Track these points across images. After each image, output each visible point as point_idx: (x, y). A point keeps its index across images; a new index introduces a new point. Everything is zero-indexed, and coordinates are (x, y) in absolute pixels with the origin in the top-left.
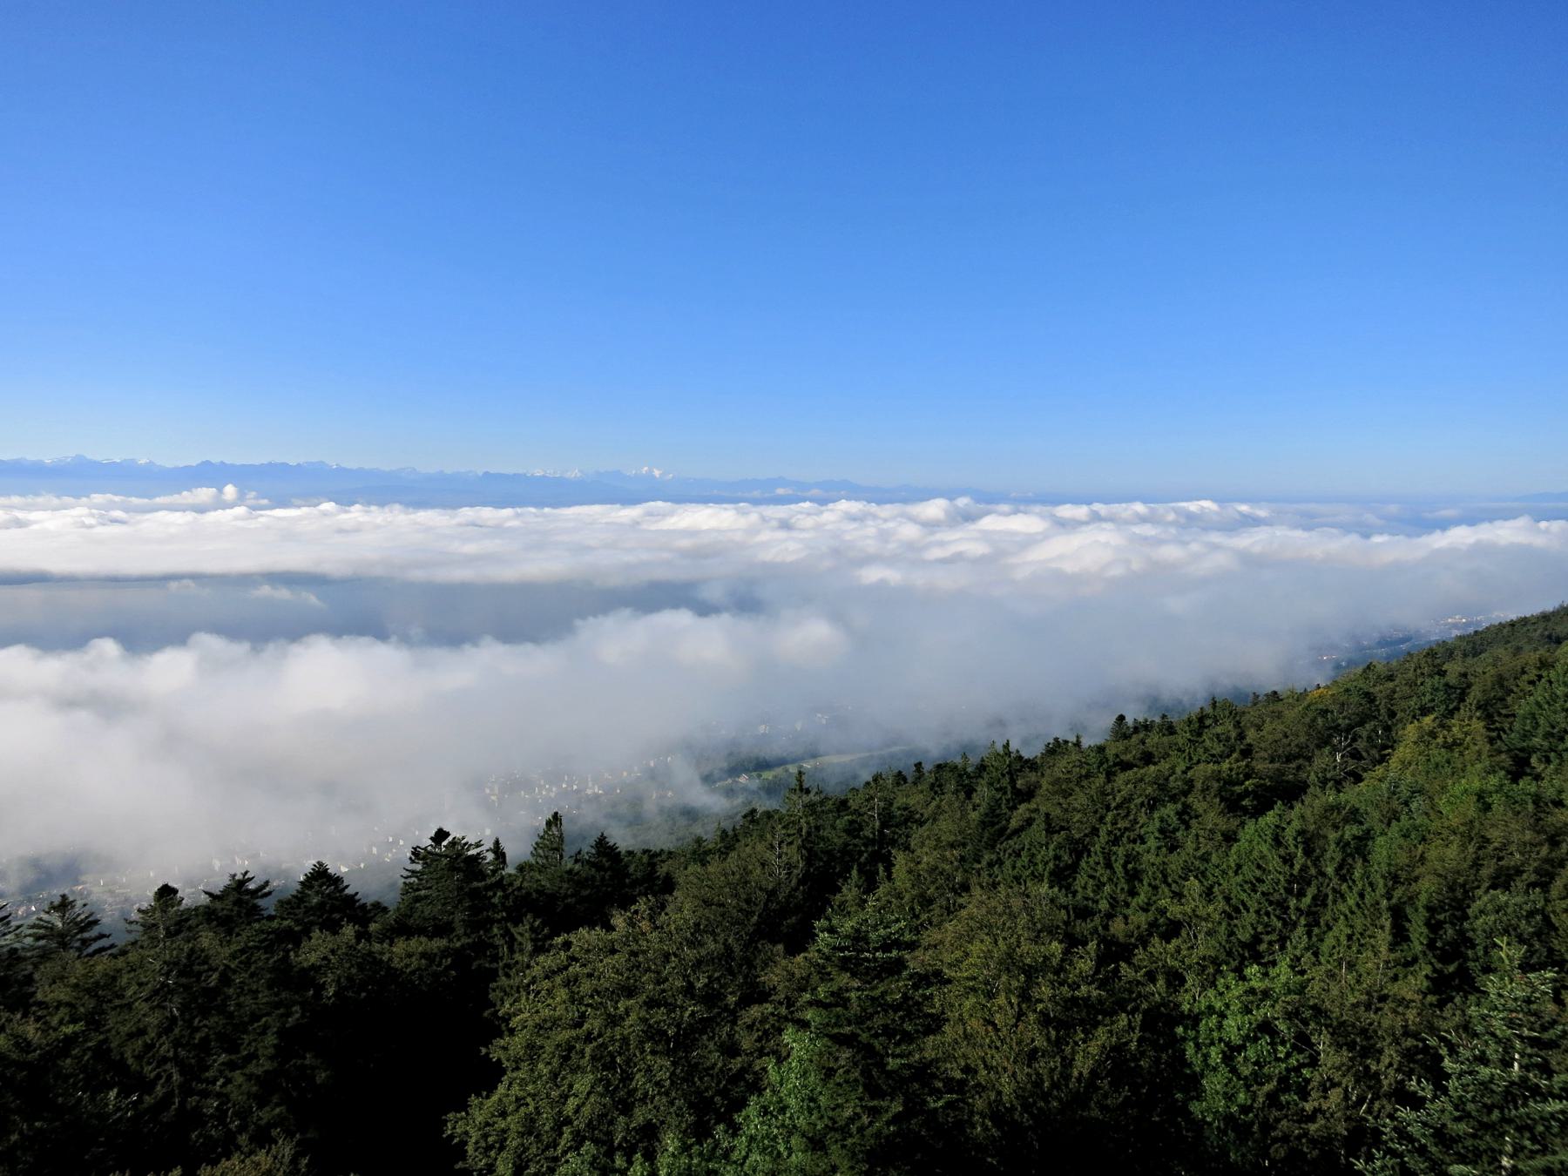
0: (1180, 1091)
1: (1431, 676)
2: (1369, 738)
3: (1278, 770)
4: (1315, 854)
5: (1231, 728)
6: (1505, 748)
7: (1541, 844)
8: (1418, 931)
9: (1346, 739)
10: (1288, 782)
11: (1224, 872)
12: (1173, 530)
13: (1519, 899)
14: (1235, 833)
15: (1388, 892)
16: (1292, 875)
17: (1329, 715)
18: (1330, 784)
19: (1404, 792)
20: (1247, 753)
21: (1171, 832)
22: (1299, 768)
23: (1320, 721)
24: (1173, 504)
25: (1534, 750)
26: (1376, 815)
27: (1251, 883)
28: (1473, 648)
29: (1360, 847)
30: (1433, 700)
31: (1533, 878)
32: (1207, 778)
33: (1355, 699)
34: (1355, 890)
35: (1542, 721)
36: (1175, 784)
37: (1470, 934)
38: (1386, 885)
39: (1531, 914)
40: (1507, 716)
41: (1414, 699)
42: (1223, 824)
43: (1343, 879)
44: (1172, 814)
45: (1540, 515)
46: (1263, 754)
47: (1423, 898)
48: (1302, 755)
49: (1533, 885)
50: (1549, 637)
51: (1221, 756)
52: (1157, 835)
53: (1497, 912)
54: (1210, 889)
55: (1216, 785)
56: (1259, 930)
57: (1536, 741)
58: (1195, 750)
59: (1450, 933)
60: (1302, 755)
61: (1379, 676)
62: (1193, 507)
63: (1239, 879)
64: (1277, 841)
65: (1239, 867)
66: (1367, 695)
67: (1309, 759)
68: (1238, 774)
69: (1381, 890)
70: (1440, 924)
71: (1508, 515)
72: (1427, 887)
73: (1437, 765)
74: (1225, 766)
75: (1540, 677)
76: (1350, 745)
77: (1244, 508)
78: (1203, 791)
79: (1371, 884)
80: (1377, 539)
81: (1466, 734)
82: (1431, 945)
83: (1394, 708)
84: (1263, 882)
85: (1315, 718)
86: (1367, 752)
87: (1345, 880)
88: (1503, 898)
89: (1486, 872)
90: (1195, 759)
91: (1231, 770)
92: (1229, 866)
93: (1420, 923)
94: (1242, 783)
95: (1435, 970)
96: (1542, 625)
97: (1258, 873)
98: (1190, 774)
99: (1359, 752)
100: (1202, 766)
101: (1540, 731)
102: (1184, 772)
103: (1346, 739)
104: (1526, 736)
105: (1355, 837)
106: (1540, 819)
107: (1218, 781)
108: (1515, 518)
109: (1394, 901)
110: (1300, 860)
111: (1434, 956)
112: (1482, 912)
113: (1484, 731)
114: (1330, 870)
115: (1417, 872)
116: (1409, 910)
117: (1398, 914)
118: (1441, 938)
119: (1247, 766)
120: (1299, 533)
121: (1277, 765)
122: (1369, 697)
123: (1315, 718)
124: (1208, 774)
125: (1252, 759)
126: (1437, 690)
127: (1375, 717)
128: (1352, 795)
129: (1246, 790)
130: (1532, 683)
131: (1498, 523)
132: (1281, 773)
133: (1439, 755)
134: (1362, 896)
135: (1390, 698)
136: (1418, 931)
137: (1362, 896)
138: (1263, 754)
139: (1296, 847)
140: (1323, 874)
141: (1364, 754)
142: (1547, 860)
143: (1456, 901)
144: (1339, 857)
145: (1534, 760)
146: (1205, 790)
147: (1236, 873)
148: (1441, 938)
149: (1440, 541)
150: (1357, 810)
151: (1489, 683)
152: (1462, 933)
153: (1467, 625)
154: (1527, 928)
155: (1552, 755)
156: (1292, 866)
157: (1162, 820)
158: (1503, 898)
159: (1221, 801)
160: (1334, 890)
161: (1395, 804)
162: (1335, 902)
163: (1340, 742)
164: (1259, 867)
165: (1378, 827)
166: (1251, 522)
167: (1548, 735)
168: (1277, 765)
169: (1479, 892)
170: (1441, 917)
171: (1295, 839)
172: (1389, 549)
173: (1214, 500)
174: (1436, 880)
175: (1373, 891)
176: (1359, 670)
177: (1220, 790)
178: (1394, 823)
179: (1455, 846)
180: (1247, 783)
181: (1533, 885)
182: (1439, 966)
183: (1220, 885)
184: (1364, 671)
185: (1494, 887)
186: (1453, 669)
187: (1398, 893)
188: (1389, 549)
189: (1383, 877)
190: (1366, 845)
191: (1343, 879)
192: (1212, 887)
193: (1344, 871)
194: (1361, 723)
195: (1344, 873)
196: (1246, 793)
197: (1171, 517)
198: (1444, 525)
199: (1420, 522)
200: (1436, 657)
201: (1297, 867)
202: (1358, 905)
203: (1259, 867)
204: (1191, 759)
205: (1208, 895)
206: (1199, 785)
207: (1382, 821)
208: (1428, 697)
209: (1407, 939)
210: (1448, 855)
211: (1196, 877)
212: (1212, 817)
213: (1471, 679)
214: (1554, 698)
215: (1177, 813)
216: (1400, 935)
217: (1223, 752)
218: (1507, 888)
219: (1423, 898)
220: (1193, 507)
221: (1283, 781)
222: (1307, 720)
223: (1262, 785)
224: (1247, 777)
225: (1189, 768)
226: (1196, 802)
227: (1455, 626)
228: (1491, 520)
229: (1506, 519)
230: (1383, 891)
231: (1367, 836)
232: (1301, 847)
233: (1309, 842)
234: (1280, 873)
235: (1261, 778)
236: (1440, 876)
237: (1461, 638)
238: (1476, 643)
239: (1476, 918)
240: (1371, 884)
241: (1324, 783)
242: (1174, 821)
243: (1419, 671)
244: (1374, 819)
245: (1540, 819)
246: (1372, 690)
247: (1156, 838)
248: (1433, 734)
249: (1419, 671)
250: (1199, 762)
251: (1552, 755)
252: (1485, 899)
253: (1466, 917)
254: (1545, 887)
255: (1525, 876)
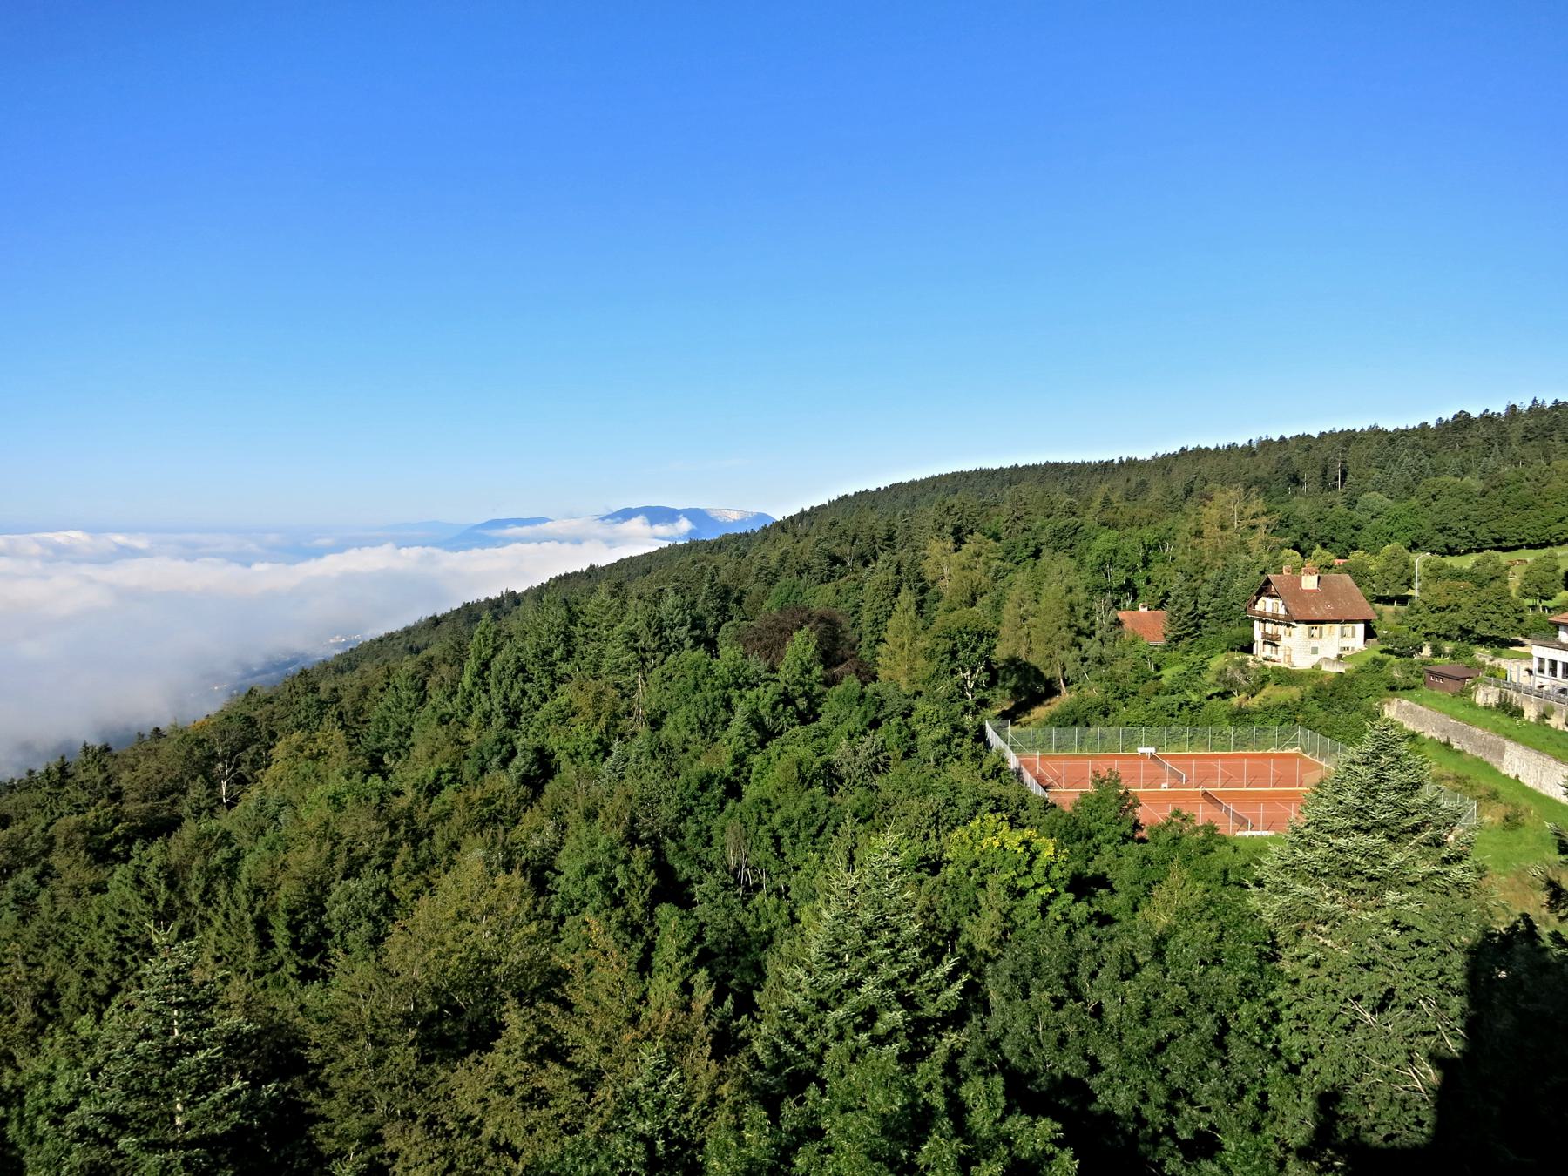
0: (1502, 969)
1: (305, 694)
2: (253, 761)
3: (150, 808)
4: (179, 886)
5: (96, 773)
6: (363, 751)
7: (383, 831)
8: (281, 935)
9: (230, 766)
10: (162, 819)
11: (85, 928)
12: (37, 565)
13: (367, 883)
14: (105, 883)
15: (251, 906)
16: (156, 913)
17: (206, 745)
18: (204, 813)
19: (272, 807)
20: (117, 796)
21: (28, 899)
22: (174, 803)
23: (197, 752)
24: (35, 535)
25: (387, 749)
26: (245, 834)
27: (115, 932)
28: (349, 664)
29: (231, 869)
30: (307, 717)
31: (379, 861)
32: (70, 832)
33: (236, 725)
34: (220, 911)
35: (391, 723)
36: (34, 846)
37: (328, 925)
38: (248, 899)
39: (376, 894)
40: (364, 722)
41: (291, 717)
42: (89, 877)
43: (208, 904)
44: (29, 879)
45: (403, 542)
46: (133, 795)
47: (282, 904)
48: (176, 789)
49: (378, 868)
50: (411, 648)
51: (87, 805)
52: (12, 905)
53: (349, 899)
54: (71, 950)
55: (81, 837)
56: (115, 978)
57: (389, 741)
58: (57, 803)
59: (311, 928)
60: (176, 789)
61: (259, 701)
62: (60, 538)
63: (102, 931)
64: (139, 882)
65: (101, 918)
66: (248, 719)
67: (184, 792)
68: (106, 821)
69: (244, 905)
70: (301, 923)
71: (374, 542)
72: (288, 892)
73: (305, 775)
74: (91, 814)
75: (388, 684)
76: (234, 771)
77: (120, 539)
78: (67, 845)
79: (234, 902)
80: (259, 567)
81: (330, 743)
82: (294, 944)
83: (274, 729)
84: (128, 927)
85: (191, 749)
86: (251, 775)
87: (211, 905)
88: (353, 886)
89: (341, 863)
90: (57, 812)
91: (97, 817)
92: (90, 921)
93: (282, 927)
94: (112, 829)
95: (299, 967)
96: (405, 639)
97: (121, 920)
98: (51, 830)
99: (244, 777)
100: (62, 821)
101: (391, 732)
102: (45, 830)
103: (230, 766)
104: (380, 738)
105: (226, 860)
106: (383, 808)
107: (84, 832)
108: (381, 545)
109: (257, 912)
110: (163, 894)
111: (298, 954)
112: (336, 902)
113: (343, 738)
114: (195, 899)
115: (279, 879)
116: (271, 918)
117: (262, 925)
118: (303, 936)
119: (115, 810)
120: (182, 563)
121: (149, 804)
122: (250, 721)
123: (191, 749)
124: (71, 827)
125: (122, 803)
126: (310, 706)
127: (257, 740)
128: (225, 821)
129: (116, 836)
130: (382, 690)
131: (366, 549)
132: (154, 810)
133: (305, 767)
134: (227, 916)
135: (270, 719)
136: (281, 935)
137: (227, 916)
138: (133, 795)
139: (158, 883)
140: (188, 904)
141: (249, 778)
142: (388, 844)
143: (316, 896)
144: (202, 884)
145: (386, 757)
146: (69, 844)
147: (99, 926)
148: (303, 936)
149: (331, 565)
150: (229, 833)
151: (356, 695)
152: (321, 926)
153: (346, 644)
154: (374, 907)
155: (402, 751)
156: (155, 905)
157: (17, 888)
158: (353, 886)
159: (86, 853)
160: (201, 917)
161: (262, 821)
162: (202, 928)
163: (224, 769)
164: (122, 913)
165: (247, 845)
166: (134, 553)
167: (398, 734)
168: (149, 804)
169: (333, 885)
170: (301, 916)
171: (157, 875)
172: (269, 576)
173: (85, 529)
174: (295, 883)
175: (237, 908)
176: (242, 697)
177: (87, 841)
178: (260, 837)
179: (312, 849)
180: (117, 828)
181: (378, 868)
182: (302, 962)
183: (81, 942)
184: (247, 696)
185: (345, 877)
186: (325, 687)
187: (260, 903)
188: (269, 576)
189: (246, 892)
190: (236, 866)
191: (208, 904)
192: (73, 947)
193: (210, 895)
194: (243, 748)
195: (208, 896)
196: (117, 839)
197: (35, 549)
198: (319, 553)
199: (299, 549)
200: (307, 679)
201: (161, 903)
202: (224, 926)
203: (122, 913)
204: (53, 813)
205: (68, 957)
206: (60, 841)
207: (250, 840)
208: (303, 714)
209: (273, 945)
210: (307, 858)
211: (55, 941)
212: (71, 868)
213: (341, 693)
214: (400, 702)
215: (35, 877)
216: (266, 943)
217: (89, 800)
218: (357, 875)
219: (282, 904)
220: (60, 538)
221: (157, 819)
222: (183, 753)
223: (133, 827)
224: (116, 822)
225: (51, 824)
226: (58, 860)
227: (336, 645)
228: (359, 547)
229: (372, 546)
230: (246, 906)
231: (238, 856)
232: (163, 882)
233: (172, 877)
234: (143, 914)
235: (131, 821)
236: (299, 878)
237: (338, 656)
238: (350, 661)
239: (333, 909)
240: (234, 902)
241: (198, 812)
242: (32, 885)
243: (293, 691)
244: (242, 837)
245: (383, 808)
246: (252, 714)
247: (12, 910)
248: (300, 749)
249: (293, 691)
250: (61, 815)
251: (402, 751)
252: (338, 890)
253: (324, 911)
254: (387, 867)
255: (372, 861)
